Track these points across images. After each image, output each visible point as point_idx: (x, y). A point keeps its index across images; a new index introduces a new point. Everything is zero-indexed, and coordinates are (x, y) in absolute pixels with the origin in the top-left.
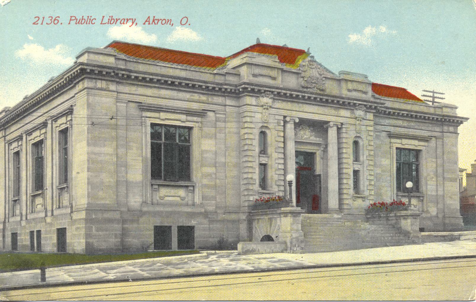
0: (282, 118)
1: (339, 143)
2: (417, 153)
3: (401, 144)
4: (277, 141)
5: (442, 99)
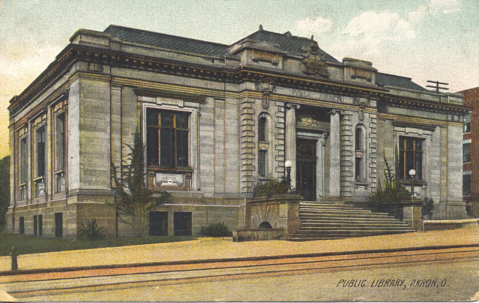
0: (283, 104)
1: (342, 131)
2: (420, 140)
3: (405, 132)
4: (276, 127)
5: (447, 89)
